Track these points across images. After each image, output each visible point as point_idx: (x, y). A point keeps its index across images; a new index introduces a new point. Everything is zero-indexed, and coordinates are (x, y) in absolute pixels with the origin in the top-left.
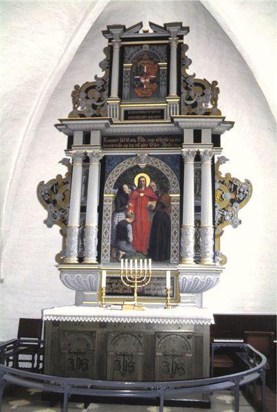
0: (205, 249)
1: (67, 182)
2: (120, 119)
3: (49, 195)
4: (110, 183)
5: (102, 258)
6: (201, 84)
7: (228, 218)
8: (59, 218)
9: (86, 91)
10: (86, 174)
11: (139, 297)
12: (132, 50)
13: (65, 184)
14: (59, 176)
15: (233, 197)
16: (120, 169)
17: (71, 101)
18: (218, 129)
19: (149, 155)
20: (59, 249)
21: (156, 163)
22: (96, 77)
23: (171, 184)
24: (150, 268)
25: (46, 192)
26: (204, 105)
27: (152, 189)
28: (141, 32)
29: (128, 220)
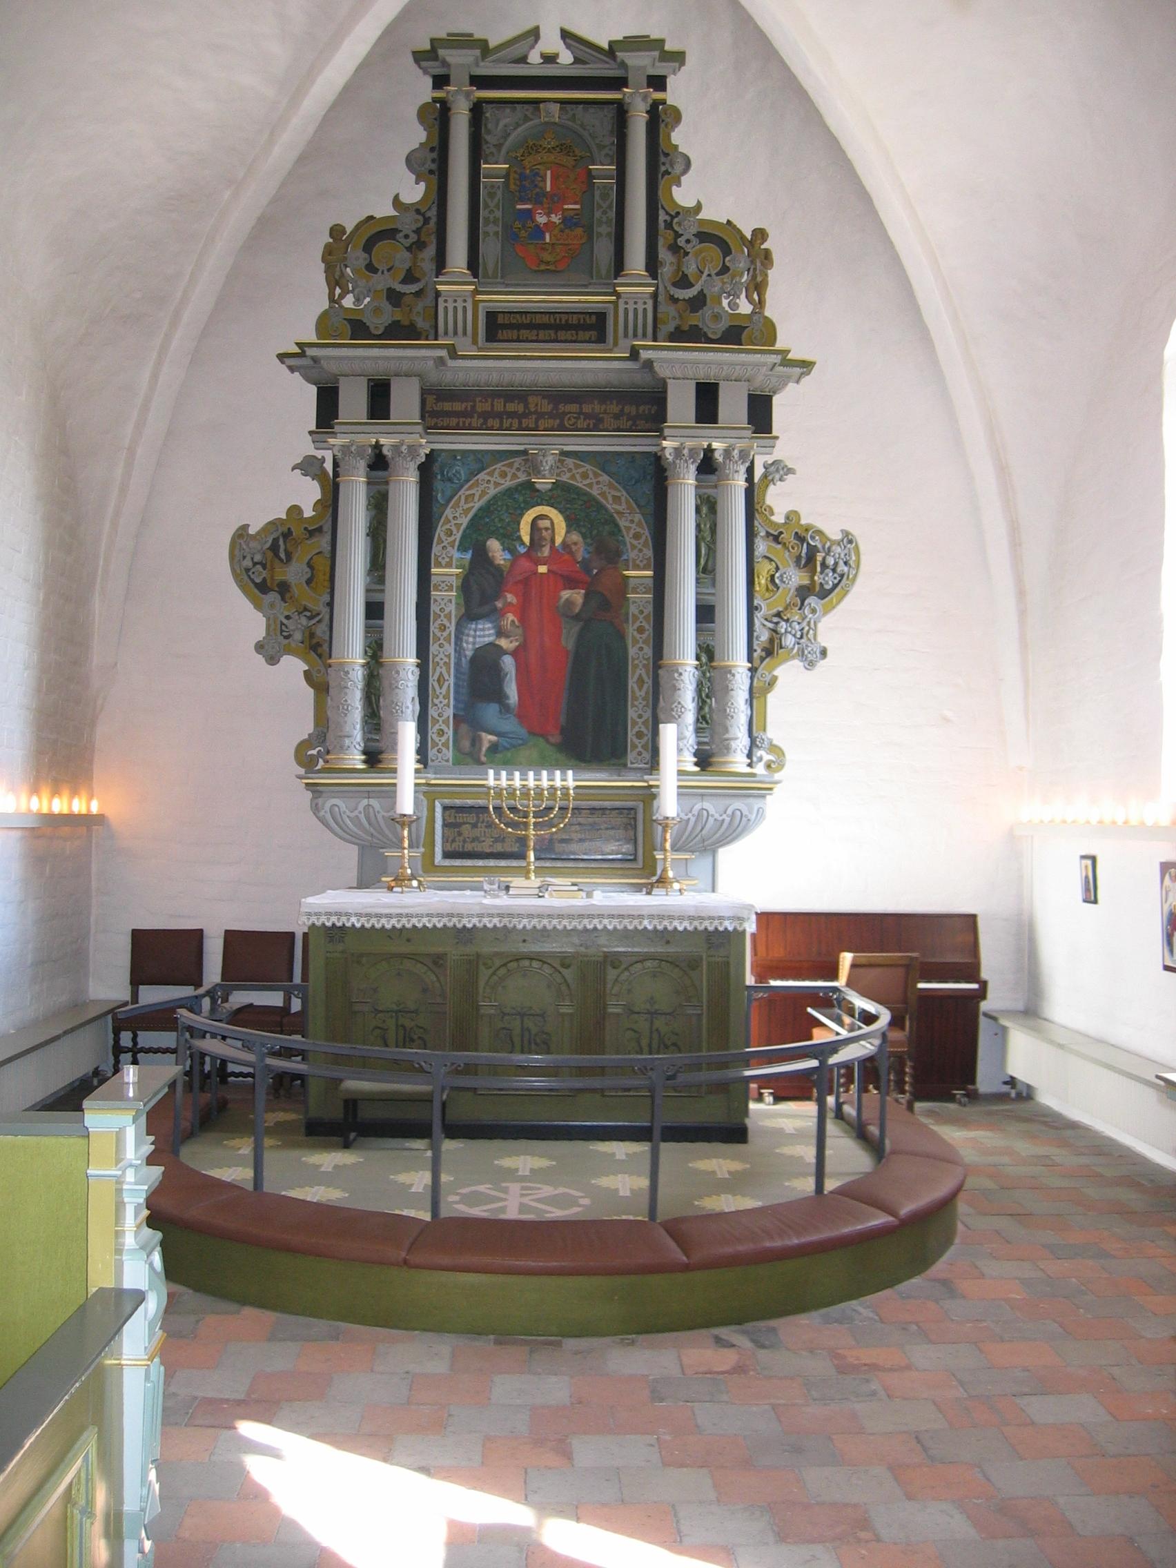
0: (726, 730)
1: (319, 530)
2: (475, 342)
3: (264, 567)
4: (449, 533)
5: (432, 753)
6: (719, 239)
7: (789, 641)
8: (298, 636)
9: (368, 247)
10: (379, 506)
11: (539, 864)
12: (508, 117)
13: (311, 533)
14: (295, 510)
15: (806, 582)
16: (477, 492)
17: (322, 277)
18: (760, 383)
19: (563, 453)
20: (306, 727)
21: (585, 476)
22: (396, 202)
23: (628, 539)
24: (571, 783)
25: (258, 558)
26: (725, 303)
27: (571, 553)
28: (534, 57)
29: (503, 643)
